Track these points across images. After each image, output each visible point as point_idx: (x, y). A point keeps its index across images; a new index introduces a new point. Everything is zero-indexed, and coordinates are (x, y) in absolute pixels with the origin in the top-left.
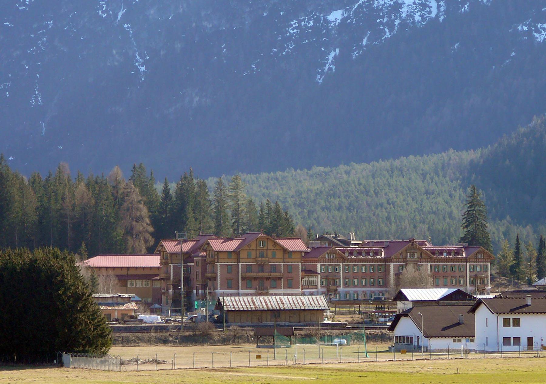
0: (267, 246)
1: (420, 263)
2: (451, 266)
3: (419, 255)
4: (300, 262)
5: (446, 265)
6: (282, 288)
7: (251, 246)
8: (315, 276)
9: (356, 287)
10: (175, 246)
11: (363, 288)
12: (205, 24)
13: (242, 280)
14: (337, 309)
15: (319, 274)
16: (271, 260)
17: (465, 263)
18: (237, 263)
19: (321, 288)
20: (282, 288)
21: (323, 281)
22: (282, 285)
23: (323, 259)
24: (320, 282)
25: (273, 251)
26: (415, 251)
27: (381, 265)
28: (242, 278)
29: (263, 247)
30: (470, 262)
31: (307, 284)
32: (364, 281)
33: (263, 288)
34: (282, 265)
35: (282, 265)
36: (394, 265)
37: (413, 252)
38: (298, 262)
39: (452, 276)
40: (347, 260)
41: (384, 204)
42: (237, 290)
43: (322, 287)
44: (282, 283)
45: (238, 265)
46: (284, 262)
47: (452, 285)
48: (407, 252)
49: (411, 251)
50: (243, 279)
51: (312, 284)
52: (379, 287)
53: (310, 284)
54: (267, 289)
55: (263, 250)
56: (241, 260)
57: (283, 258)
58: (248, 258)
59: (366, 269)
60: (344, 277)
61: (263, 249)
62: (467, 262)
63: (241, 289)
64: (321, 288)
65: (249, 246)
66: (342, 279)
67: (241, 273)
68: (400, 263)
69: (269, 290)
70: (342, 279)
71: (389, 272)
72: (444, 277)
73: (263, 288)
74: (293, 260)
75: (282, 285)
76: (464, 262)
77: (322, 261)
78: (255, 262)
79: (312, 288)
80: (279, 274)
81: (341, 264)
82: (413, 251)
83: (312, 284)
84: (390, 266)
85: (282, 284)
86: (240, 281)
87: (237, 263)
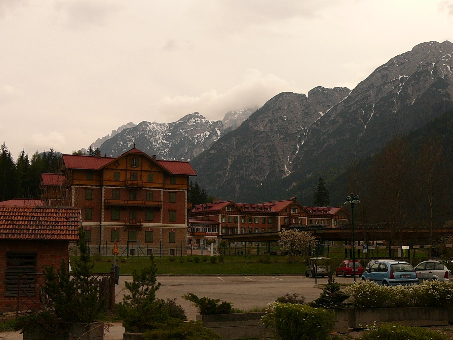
0: (142, 167)
4: (187, 190)
6: (161, 221)
7: (119, 165)
8: (216, 225)
12: (207, 188)
13: (105, 209)
15: (220, 223)
16: (145, 185)
18: (100, 187)
20: (161, 221)
22: (162, 218)
23: (224, 211)
25: (149, 173)
27: (270, 218)
28: (105, 206)
29: (137, 167)
30: (334, 218)
31: (210, 232)
33: (134, 221)
34: (162, 192)
35: (162, 192)
38: (183, 190)
40: (244, 213)
42: (100, 223)
44: (162, 215)
45: (101, 189)
46: (166, 189)
50: (107, 208)
51: (214, 232)
53: (212, 232)
54: (140, 222)
55: (136, 170)
56: (105, 183)
57: (163, 184)
58: (114, 181)
60: (241, 227)
61: (136, 169)
62: (332, 218)
63: (104, 221)
65: (117, 164)
66: (239, 228)
67: (105, 200)
68: (229, 215)
69: (143, 224)
70: (239, 228)
73: (134, 221)
74: (179, 187)
75: (162, 218)
76: (330, 218)
77: (225, 213)
78: (123, 186)
79: (214, 235)
80: (157, 203)
81: (239, 216)
83: (214, 232)
84: (277, 219)
85: (162, 217)
86: (103, 211)
87: (100, 187)
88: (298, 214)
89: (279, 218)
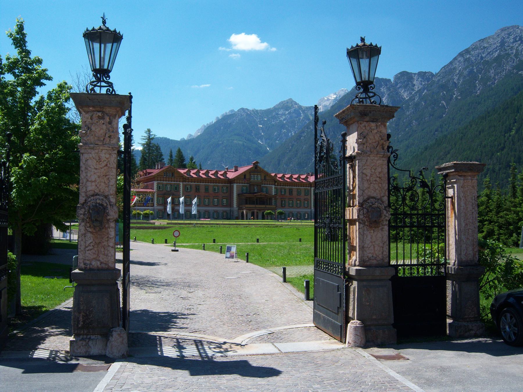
1: (264, 185)
2: (222, 187)
3: (263, 178)
5: (218, 186)
9: (208, 206)
10: (171, 152)
11: (205, 207)
14: (69, 225)
17: (310, 188)
19: (157, 206)
21: (188, 200)
24: (157, 200)
26: (259, 174)
32: (207, 200)
36: (237, 186)
37: (257, 175)
39: (297, 199)
41: (341, 140)
43: (158, 204)
47: (290, 207)
48: (250, 174)
49: (254, 173)
52: (223, 206)
59: (218, 189)
64: (157, 206)
71: (233, 193)
72: (204, 196)
77: (266, 183)
82: (256, 174)
88: (261, 181)
89: (235, 185)
